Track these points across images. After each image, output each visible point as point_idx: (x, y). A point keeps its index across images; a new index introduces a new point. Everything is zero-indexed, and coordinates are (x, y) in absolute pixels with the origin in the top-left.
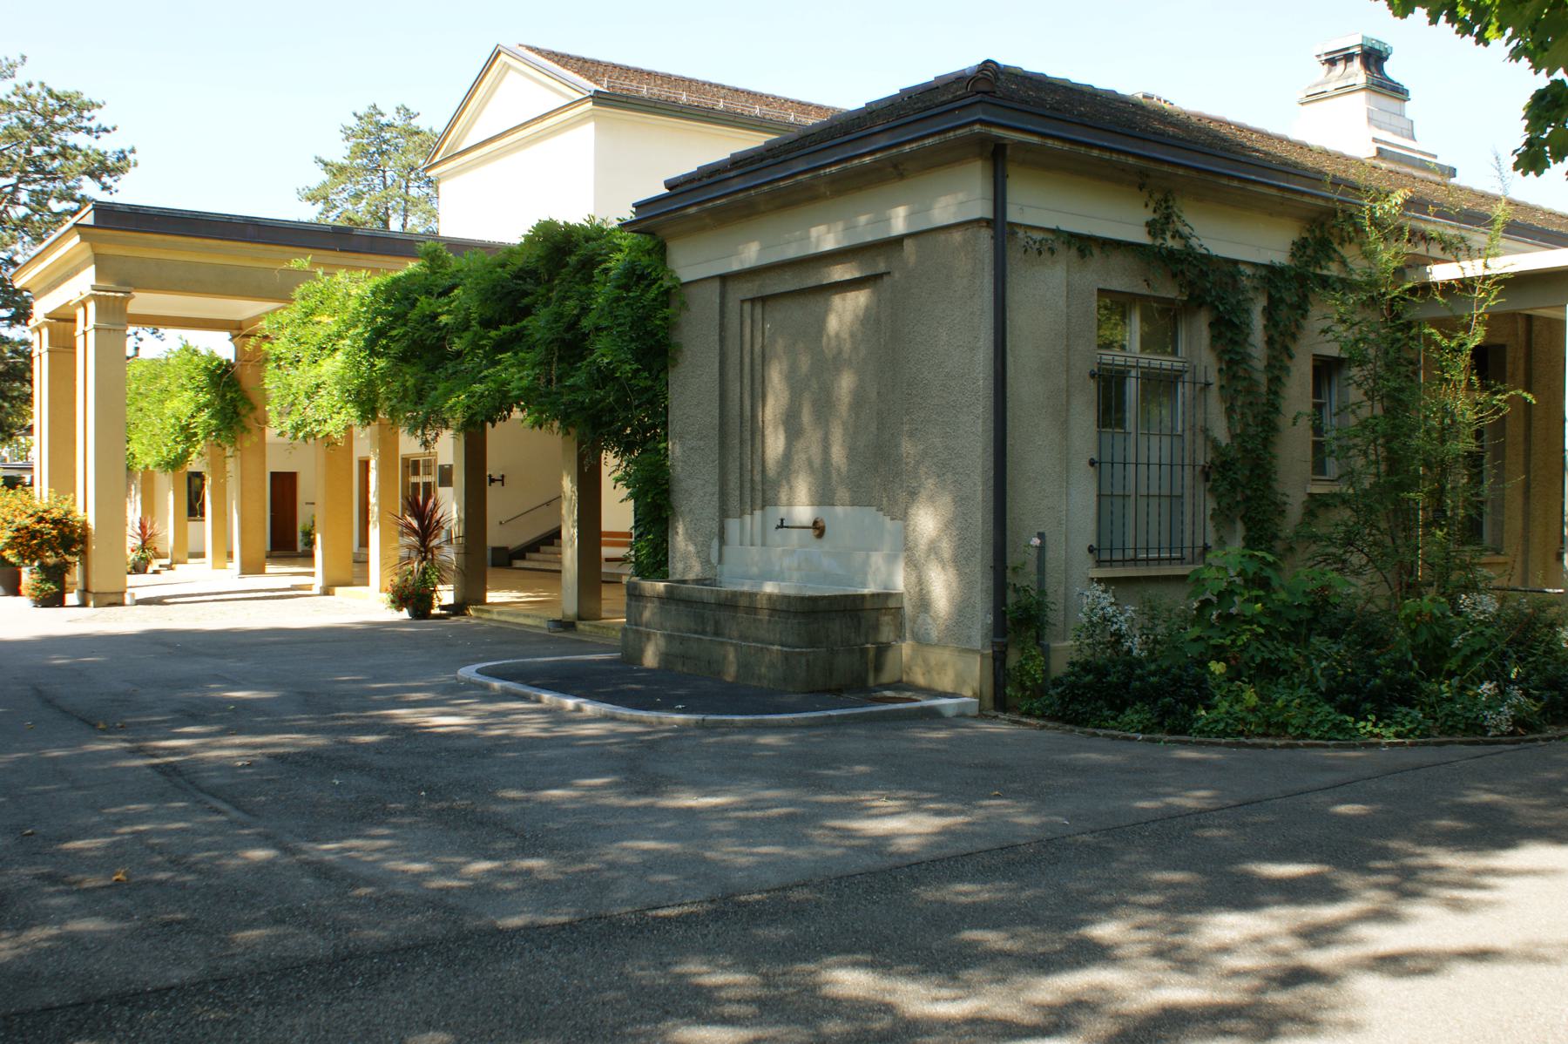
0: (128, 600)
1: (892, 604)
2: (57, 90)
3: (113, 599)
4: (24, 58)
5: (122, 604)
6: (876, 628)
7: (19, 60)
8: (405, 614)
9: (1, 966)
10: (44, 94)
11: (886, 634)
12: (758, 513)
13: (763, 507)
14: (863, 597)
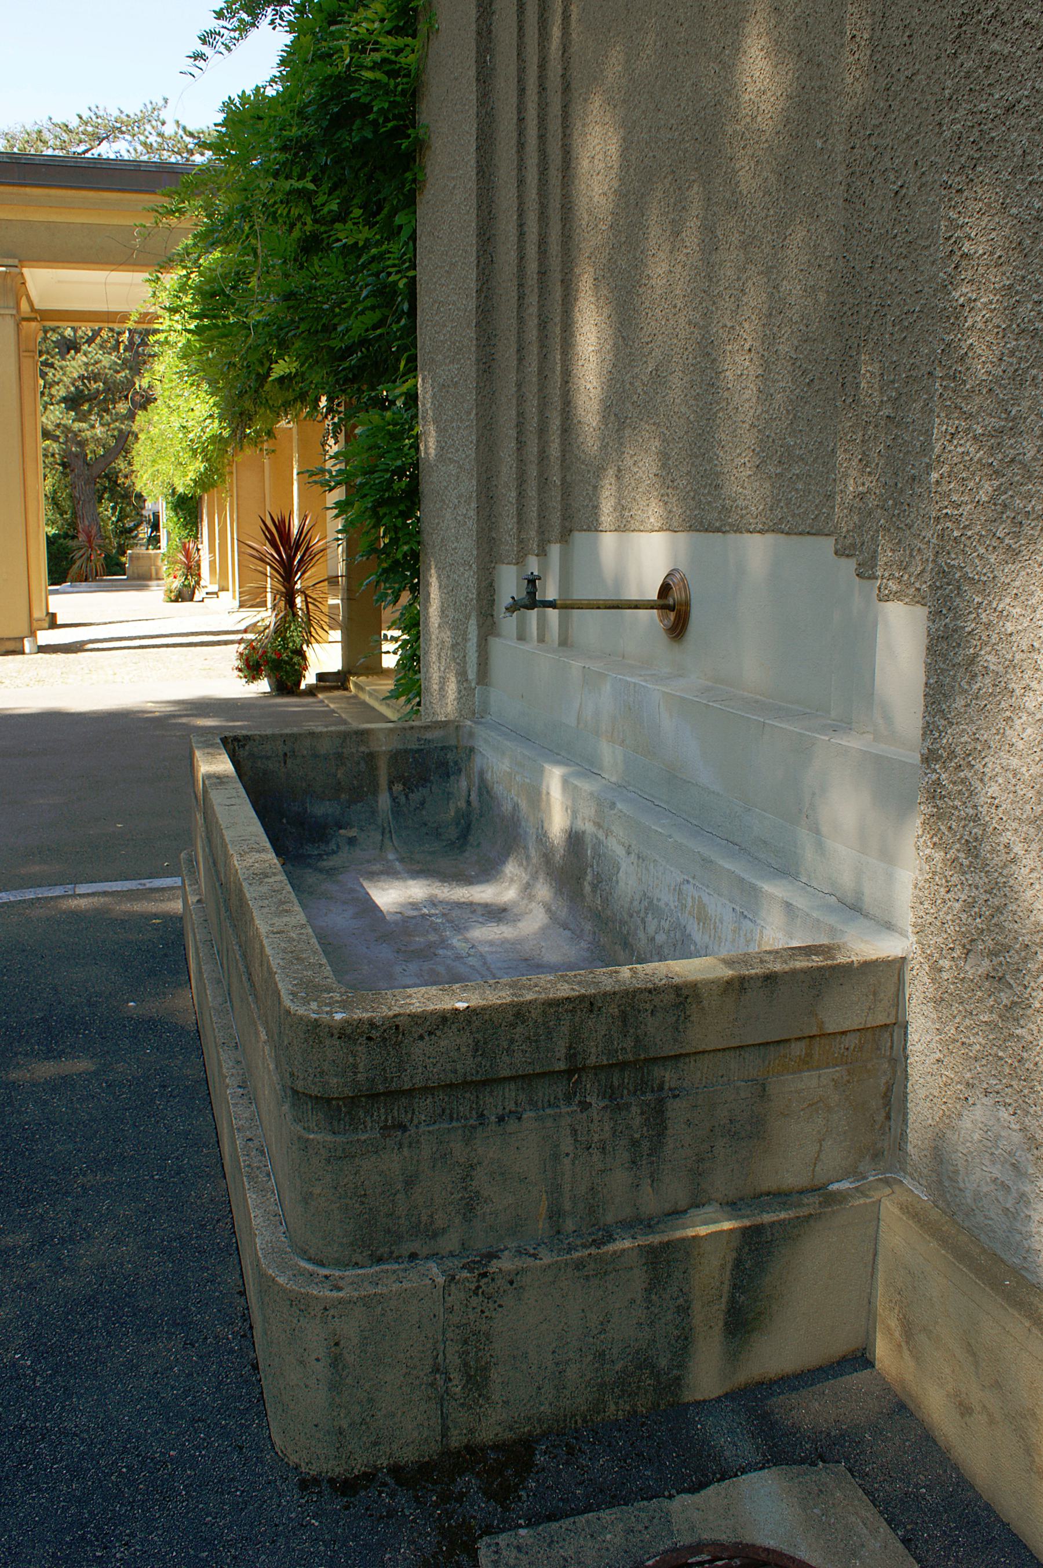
0: (27, 645)
1: (843, 1014)
2: (191, 128)
3: (10, 646)
4: (166, 101)
5: (23, 653)
6: (751, 1130)
7: (161, 103)
8: (263, 685)
9: (1042, 551)
10: (181, 132)
11: (803, 1147)
12: (555, 550)
13: (565, 536)
14: (683, 997)
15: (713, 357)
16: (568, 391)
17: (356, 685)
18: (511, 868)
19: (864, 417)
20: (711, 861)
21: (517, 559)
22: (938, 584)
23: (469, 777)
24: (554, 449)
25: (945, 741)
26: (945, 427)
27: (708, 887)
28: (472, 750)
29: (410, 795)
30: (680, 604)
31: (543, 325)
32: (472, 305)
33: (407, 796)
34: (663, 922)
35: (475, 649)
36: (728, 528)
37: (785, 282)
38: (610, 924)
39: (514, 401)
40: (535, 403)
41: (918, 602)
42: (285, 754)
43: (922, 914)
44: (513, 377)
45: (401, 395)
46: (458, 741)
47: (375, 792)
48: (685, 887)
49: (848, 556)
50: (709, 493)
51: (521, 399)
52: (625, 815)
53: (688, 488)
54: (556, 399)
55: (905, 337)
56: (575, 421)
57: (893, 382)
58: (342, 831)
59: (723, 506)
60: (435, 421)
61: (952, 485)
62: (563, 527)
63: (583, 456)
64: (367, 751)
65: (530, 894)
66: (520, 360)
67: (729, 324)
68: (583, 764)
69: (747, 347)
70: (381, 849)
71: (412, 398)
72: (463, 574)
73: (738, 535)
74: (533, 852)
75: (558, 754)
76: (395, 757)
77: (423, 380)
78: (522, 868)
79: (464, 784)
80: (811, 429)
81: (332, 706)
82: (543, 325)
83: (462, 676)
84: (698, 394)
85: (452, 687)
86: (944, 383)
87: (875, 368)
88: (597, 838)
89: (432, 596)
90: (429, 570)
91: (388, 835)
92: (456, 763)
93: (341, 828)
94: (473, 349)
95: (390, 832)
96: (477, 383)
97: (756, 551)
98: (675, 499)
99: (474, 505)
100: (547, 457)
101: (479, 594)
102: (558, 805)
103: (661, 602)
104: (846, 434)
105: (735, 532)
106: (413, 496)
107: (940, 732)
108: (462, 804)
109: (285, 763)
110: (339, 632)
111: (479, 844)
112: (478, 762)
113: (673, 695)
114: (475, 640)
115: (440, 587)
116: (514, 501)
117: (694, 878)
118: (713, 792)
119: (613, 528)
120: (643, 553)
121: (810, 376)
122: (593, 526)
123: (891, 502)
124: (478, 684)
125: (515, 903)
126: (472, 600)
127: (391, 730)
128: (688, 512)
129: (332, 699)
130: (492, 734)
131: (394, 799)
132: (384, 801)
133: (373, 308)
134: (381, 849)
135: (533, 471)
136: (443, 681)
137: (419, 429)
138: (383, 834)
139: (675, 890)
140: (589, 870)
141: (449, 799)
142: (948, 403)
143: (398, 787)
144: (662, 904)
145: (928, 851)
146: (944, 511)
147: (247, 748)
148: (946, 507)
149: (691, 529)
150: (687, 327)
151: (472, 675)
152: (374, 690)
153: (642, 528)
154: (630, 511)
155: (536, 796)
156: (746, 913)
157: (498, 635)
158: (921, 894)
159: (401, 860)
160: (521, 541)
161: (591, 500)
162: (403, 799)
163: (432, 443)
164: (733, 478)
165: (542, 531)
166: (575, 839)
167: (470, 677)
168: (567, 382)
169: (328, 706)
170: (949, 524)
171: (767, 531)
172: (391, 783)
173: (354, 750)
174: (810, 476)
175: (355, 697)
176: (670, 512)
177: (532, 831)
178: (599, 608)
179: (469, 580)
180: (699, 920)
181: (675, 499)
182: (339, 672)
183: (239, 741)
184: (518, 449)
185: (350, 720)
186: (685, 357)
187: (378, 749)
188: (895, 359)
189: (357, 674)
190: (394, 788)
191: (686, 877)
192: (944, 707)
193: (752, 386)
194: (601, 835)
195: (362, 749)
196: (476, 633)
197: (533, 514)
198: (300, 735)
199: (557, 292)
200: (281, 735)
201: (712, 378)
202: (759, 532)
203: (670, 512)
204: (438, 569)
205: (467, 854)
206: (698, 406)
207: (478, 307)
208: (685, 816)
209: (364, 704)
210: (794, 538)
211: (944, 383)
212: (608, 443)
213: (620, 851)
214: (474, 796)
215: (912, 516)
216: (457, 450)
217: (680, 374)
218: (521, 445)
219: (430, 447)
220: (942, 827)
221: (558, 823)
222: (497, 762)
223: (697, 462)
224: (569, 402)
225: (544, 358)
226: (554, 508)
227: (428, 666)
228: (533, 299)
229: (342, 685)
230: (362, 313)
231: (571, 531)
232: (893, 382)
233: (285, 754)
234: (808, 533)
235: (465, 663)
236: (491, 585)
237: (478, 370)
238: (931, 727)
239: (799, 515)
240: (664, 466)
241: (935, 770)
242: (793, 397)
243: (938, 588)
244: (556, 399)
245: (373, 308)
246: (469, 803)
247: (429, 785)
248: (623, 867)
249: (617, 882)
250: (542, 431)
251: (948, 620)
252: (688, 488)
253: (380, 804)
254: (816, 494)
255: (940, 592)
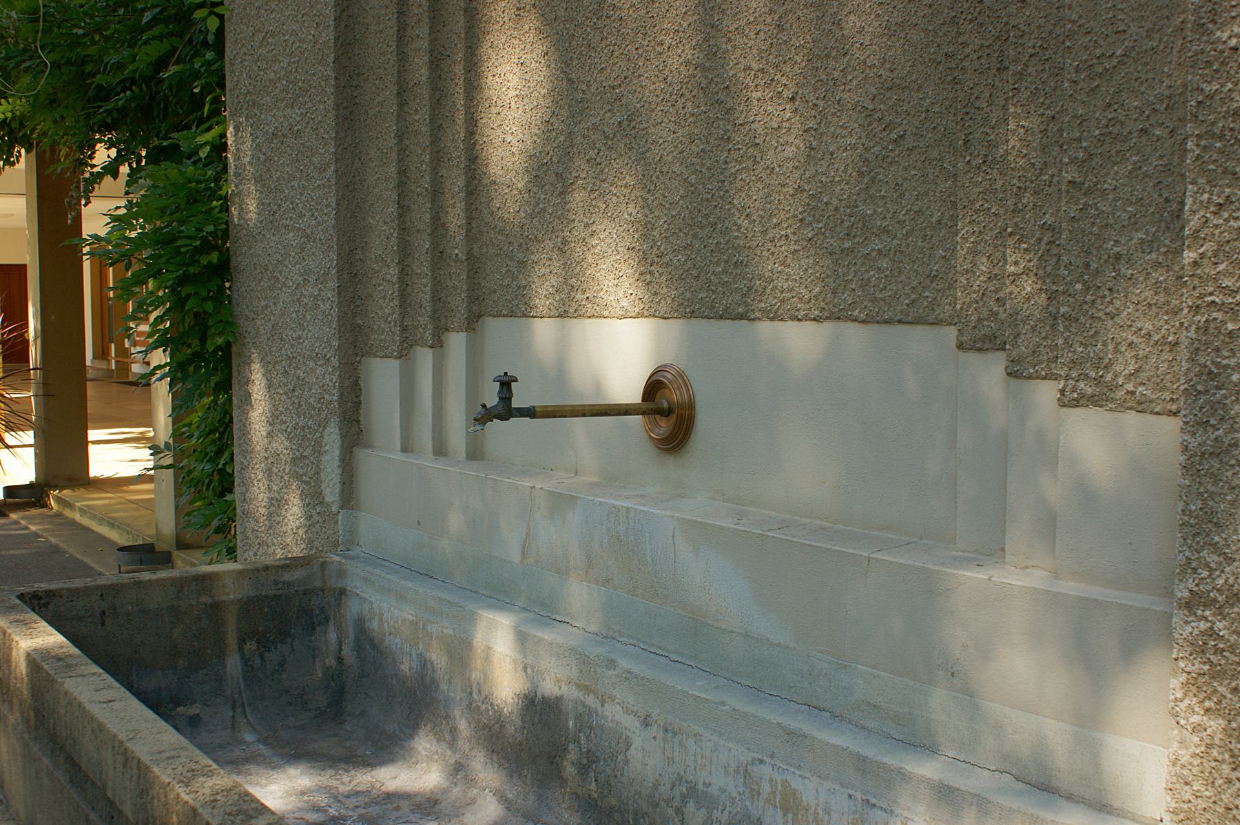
12: (457, 342)
13: (472, 322)
15: (728, 106)
16: (474, 144)
17: (59, 500)
18: (423, 744)
19: (1015, 181)
20: (804, 735)
21: (400, 352)
22: (1199, 388)
23: (339, 627)
24: (455, 218)
25: (1221, 581)
26: (1206, 196)
27: (799, 767)
28: (343, 592)
29: (267, 654)
30: (681, 406)
31: (437, 62)
32: (328, 35)
33: (262, 656)
34: (716, 814)
35: (336, 463)
36: (758, 315)
37: (852, 17)
38: (617, 816)
39: (394, 156)
40: (427, 158)
41: (1130, 408)
42: (103, 613)
43: (1188, 796)
44: (391, 125)
45: (206, 143)
46: (324, 582)
47: (222, 657)
48: (755, 769)
49: (980, 350)
50: (725, 271)
51: (403, 153)
52: (637, 676)
53: (689, 264)
54: (457, 154)
55: (1097, 86)
56: (486, 181)
57: (1079, 140)
58: (180, 709)
59: (750, 289)
60: (258, 179)
61: (1221, 267)
62: (470, 311)
63: (500, 225)
64: (210, 601)
65: (466, 777)
66: (402, 104)
67: (755, 66)
68: (539, 608)
69: (787, 93)
70: (233, 728)
71: (220, 147)
72: (313, 370)
73: (776, 323)
74: (463, 726)
75: (500, 594)
76: (248, 606)
77: (237, 129)
78: (444, 744)
79: (333, 636)
80: (902, 195)
81: (33, 528)
82: (437, 62)
83: (313, 497)
84: (703, 150)
85: (294, 512)
86: (1203, 143)
87: (1034, 122)
88: (585, 706)
89: (255, 396)
90: (248, 362)
91: (240, 710)
92: (322, 609)
93: (179, 705)
94: (330, 90)
95: (243, 705)
96: (337, 133)
97: (799, 342)
98: (664, 278)
99: (333, 284)
100: (443, 225)
101: (342, 395)
102: (503, 660)
103: (650, 405)
104: (972, 202)
105: (772, 319)
106: (223, 269)
107: (1211, 570)
108: (331, 661)
109: (103, 625)
110: (31, 433)
111: (363, 713)
112: (352, 608)
113: (696, 522)
114: (337, 453)
115: (269, 387)
116: (395, 279)
117: (772, 756)
118: (779, 645)
119: (554, 312)
120: (619, 347)
121: (899, 131)
122: (520, 309)
123: (1079, 286)
124: (341, 508)
125: (445, 791)
126: (331, 402)
127: (240, 572)
128: (688, 295)
129: (31, 519)
130: (377, 571)
131: (246, 661)
132: (233, 664)
133: (160, 38)
134: (233, 728)
135: (423, 243)
136: (277, 504)
137: (230, 189)
138: (234, 708)
139: (736, 771)
140: (571, 746)
141: (314, 657)
142: (1212, 167)
143: (251, 646)
144: (714, 790)
145: (1195, 719)
146: (1210, 299)
147: (51, 607)
148: (1211, 294)
149: (684, 316)
150: (682, 68)
151: (331, 494)
152: (88, 506)
153: (606, 313)
154: (584, 291)
155: (461, 650)
156: (873, 801)
157: (369, 446)
158: (1185, 772)
159: (265, 741)
160: (404, 329)
161: (514, 278)
162: (257, 661)
163: (252, 206)
164: (765, 253)
165: (436, 317)
166: (537, 708)
167: (328, 499)
168: (472, 133)
169: (26, 528)
170: (1219, 315)
171: (827, 318)
172: (242, 641)
173: (193, 602)
174: (901, 252)
175: (59, 515)
176: (655, 294)
177: (458, 695)
178: (584, 415)
179: (324, 380)
180: (785, 810)
181: (664, 278)
182: (31, 485)
183: (40, 598)
184: (400, 215)
185: (63, 546)
186: (679, 104)
187: (224, 598)
188: (1080, 112)
189: (55, 487)
190: (246, 647)
191: (757, 756)
192: (1217, 539)
193: (797, 141)
194: (591, 701)
195: (204, 599)
196: (337, 444)
197: (423, 294)
198: (123, 585)
199: (458, 25)
200: (97, 587)
201: (726, 131)
202: (814, 319)
203: (655, 294)
204: (265, 363)
205: (348, 727)
206: (703, 165)
207: (336, 39)
208: (726, 675)
209: (73, 523)
210: (870, 326)
211: (1203, 143)
212: (544, 210)
213: (630, 723)
214: (346, 651)
215: (1117, 303)
216: (302, 216)
217: (671, 125)
218: (403, 209)
219: (249, 207)
220: (1219, 689)
221: (506, 685)
222: (389, 608)
223: (702, 234)
224: (476, 158)
225: (438, 102)
226: (455, 288)
227: (247, 485)
228: (422, 31)
229: (38, 501)
230: (146, 43)
231: (480, 316)
232: (1079, 140)
233: (103, 613)
234: (900, 321)
235: (319, 482)
236: (356, 383)
237: (337, 117)
238: (1194, 565)
239: (883, 299)
240: (645, 237)
241: (1206, 619)
242: (870, 156)
243: (1200, 392)
244: (457, 154)
245: (160, 38)
246: (340, 659)
247: (289, 640)
248: (637, 742)
249: (627, 762)
250: (436, 193)
251: (1220, 432)
252: (689, 264)
253: (228, 669)
254: (912, 275)
255: (1203, 398)
